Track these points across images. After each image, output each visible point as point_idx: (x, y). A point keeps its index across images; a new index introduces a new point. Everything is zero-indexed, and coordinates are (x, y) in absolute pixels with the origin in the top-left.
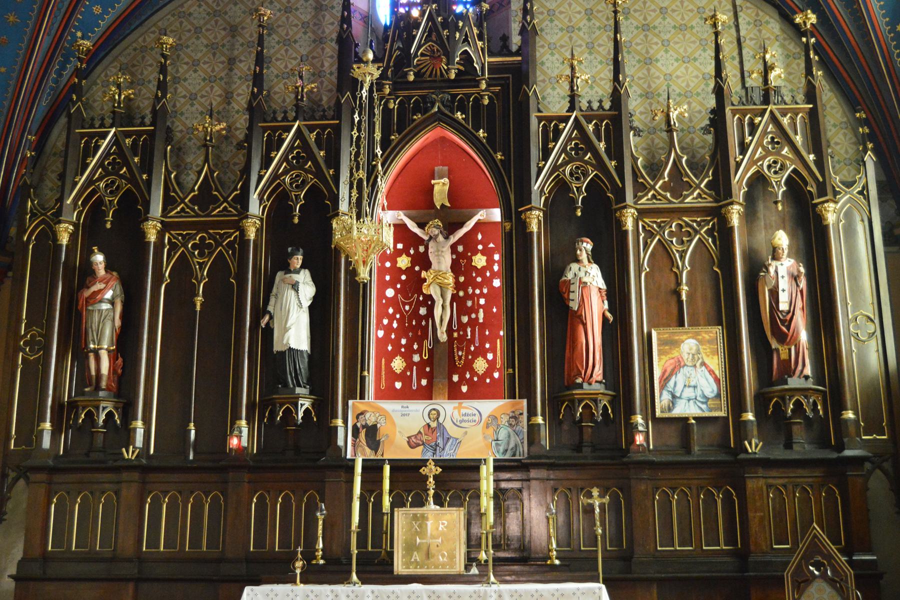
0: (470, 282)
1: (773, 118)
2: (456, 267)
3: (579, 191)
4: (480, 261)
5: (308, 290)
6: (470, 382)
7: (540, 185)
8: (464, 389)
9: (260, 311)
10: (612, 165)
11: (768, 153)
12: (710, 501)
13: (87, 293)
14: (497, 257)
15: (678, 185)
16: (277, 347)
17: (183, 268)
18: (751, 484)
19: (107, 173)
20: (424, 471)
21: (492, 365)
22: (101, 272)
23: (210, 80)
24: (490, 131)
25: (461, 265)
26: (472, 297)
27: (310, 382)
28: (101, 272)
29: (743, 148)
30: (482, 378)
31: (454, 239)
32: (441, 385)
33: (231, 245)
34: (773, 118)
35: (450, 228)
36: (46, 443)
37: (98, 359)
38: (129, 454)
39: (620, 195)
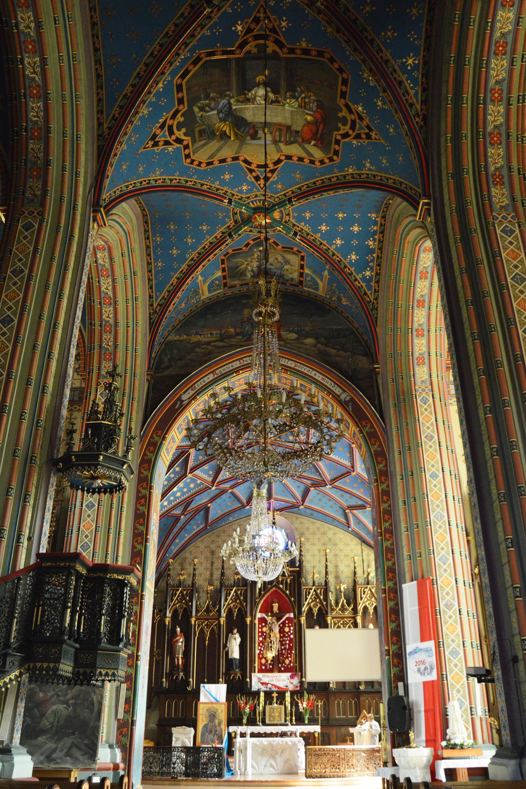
0: (284, 636)
1: (370, 590)
2: (280, 632)
3: (315, 611)
4: (287, 629)
5: (239, 640)
6: (284, 667)
7: (305, 609)
8: (283, 669)
9: (225, 646)
10: (325, 603)
11: (368, 600)
12: (351, 703)
13: (175, 640)
14: (292, 628)
15: (343, 609)
16: (230, 657)
17: (202, 632)
18: (361, 698)
19: (179, 602)
20: (273, 695)
21: (290, 662)
22: (179, 633)
23: (206, 569)
24: (290, 591)
25: (281, 631)
26: (285, 641)
27: (239, 667)
28: (179, 633)
29: (361, 598)
30: (288, 665)
31: (279, 623)
32: (276, 668)
33: (216, 625)
34: (370, 590)
35: (278, 620)
36: (164, 686)
37: (178, 660)
38: (189, 689)
39: (327, 613)
